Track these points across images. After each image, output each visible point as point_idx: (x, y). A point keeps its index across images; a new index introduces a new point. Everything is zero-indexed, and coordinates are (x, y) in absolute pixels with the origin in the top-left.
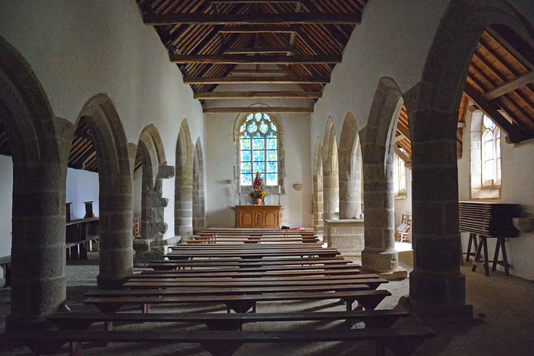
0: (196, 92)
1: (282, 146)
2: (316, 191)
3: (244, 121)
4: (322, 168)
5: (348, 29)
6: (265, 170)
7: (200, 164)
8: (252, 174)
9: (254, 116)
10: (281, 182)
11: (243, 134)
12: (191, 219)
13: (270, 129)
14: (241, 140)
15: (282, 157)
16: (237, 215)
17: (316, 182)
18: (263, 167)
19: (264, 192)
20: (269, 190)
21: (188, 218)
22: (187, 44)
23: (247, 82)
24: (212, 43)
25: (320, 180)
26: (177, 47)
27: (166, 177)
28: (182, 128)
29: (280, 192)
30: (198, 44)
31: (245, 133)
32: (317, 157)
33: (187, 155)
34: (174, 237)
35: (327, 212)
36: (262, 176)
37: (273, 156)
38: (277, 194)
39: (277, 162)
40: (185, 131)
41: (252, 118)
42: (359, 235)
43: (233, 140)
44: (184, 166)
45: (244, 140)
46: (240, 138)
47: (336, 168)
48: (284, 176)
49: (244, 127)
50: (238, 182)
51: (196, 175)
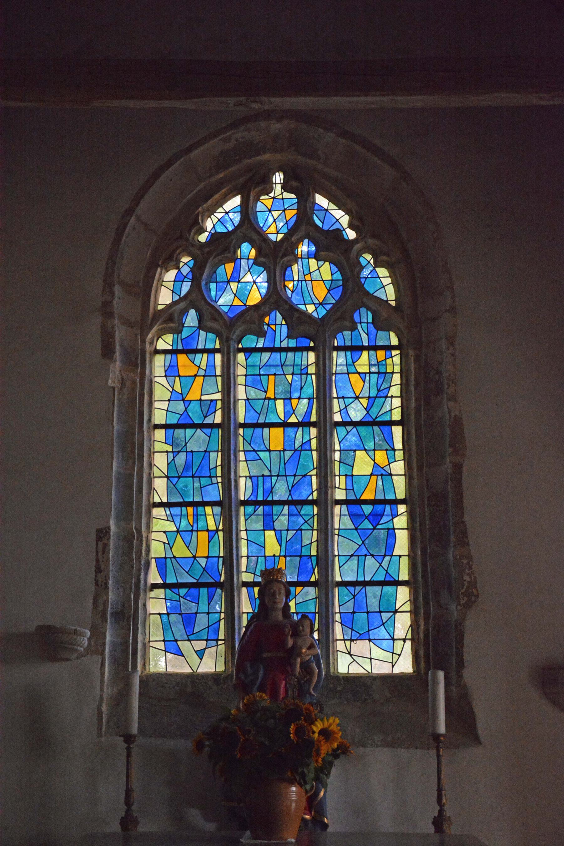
1: (439, 391)
3: (181, 237)
5: (104, 729)
11: (170, 319)
15: (447, 466)
19: (333, 723)
29: (442, 729)
31: (185, 312)
41: (236, 218)
43: (98, 351)
46: (148, 348)
48: (468, 606)
49: (179, 279)
50: (125, 643)
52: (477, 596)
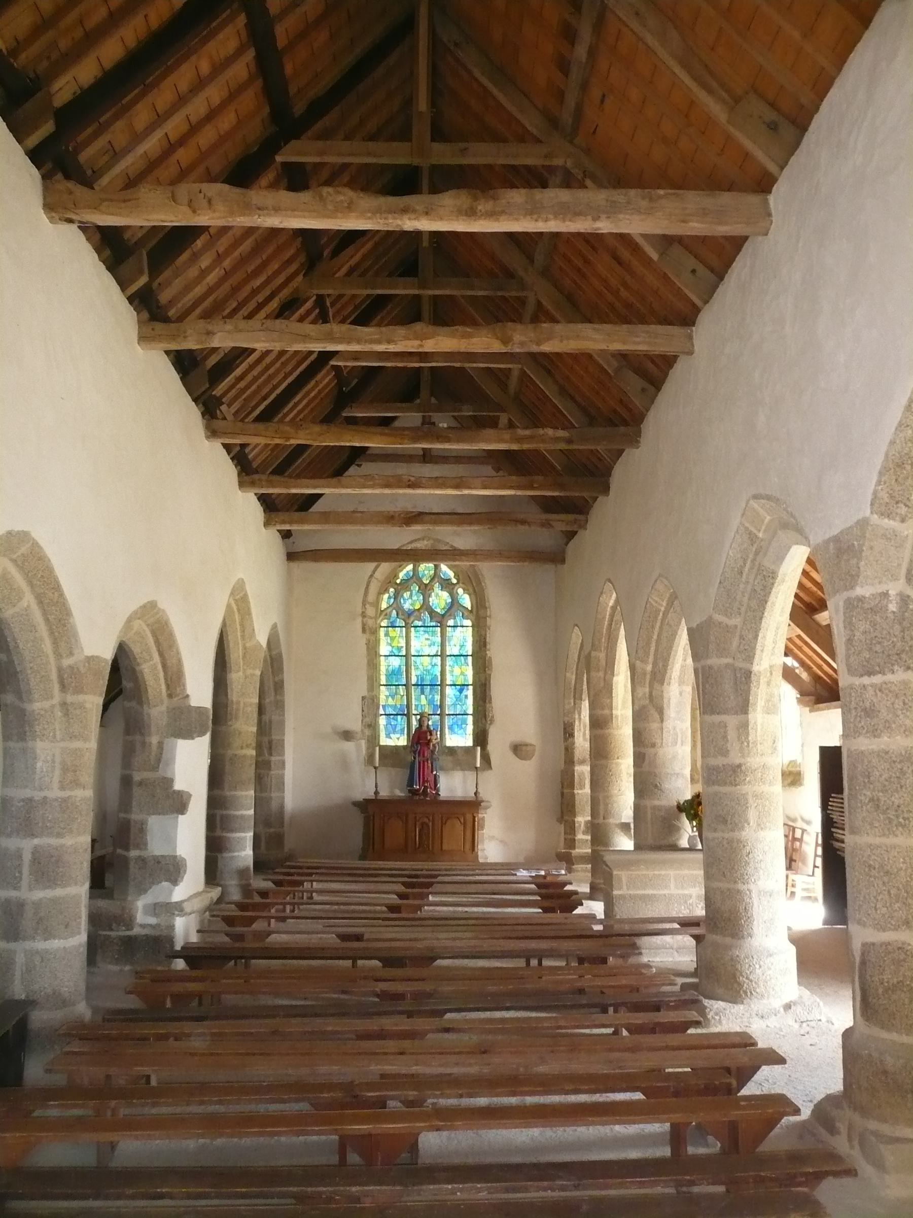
0: (269, 504)
2: (570, 761)
4: (585, 705)
6: (442, 706)
7: (276, 690)
8: (408, 716)
9: (415, 570)
10: (481, 738)
12: (250, 835)
13: (454, 604)
14: (382, 629)
16: (368, 823)
17: (570, 740)
18: (437, 697)
20: (450, 758)
21: (243, 835)
22: (248, 392)
23: (401, 491)
24: (313, 389)
25: (581, 734)
26: (224, 400)
27: (188, 734)
28: (233, 602)
29: (478, 765)
30: (278, 391)
32: (574, 677)
33: (244, 670)
34: (203, 891)
35: (601, 821)
36: (432, 722)
37: (464, 672)
38: (470, 769)
39: (471, 688)
40: (239, 610)
42: (686, 892)
44: (234, 700)
45: (390, 629)
47: (624, 707)
49: (389, 598)
51: (265, 718)
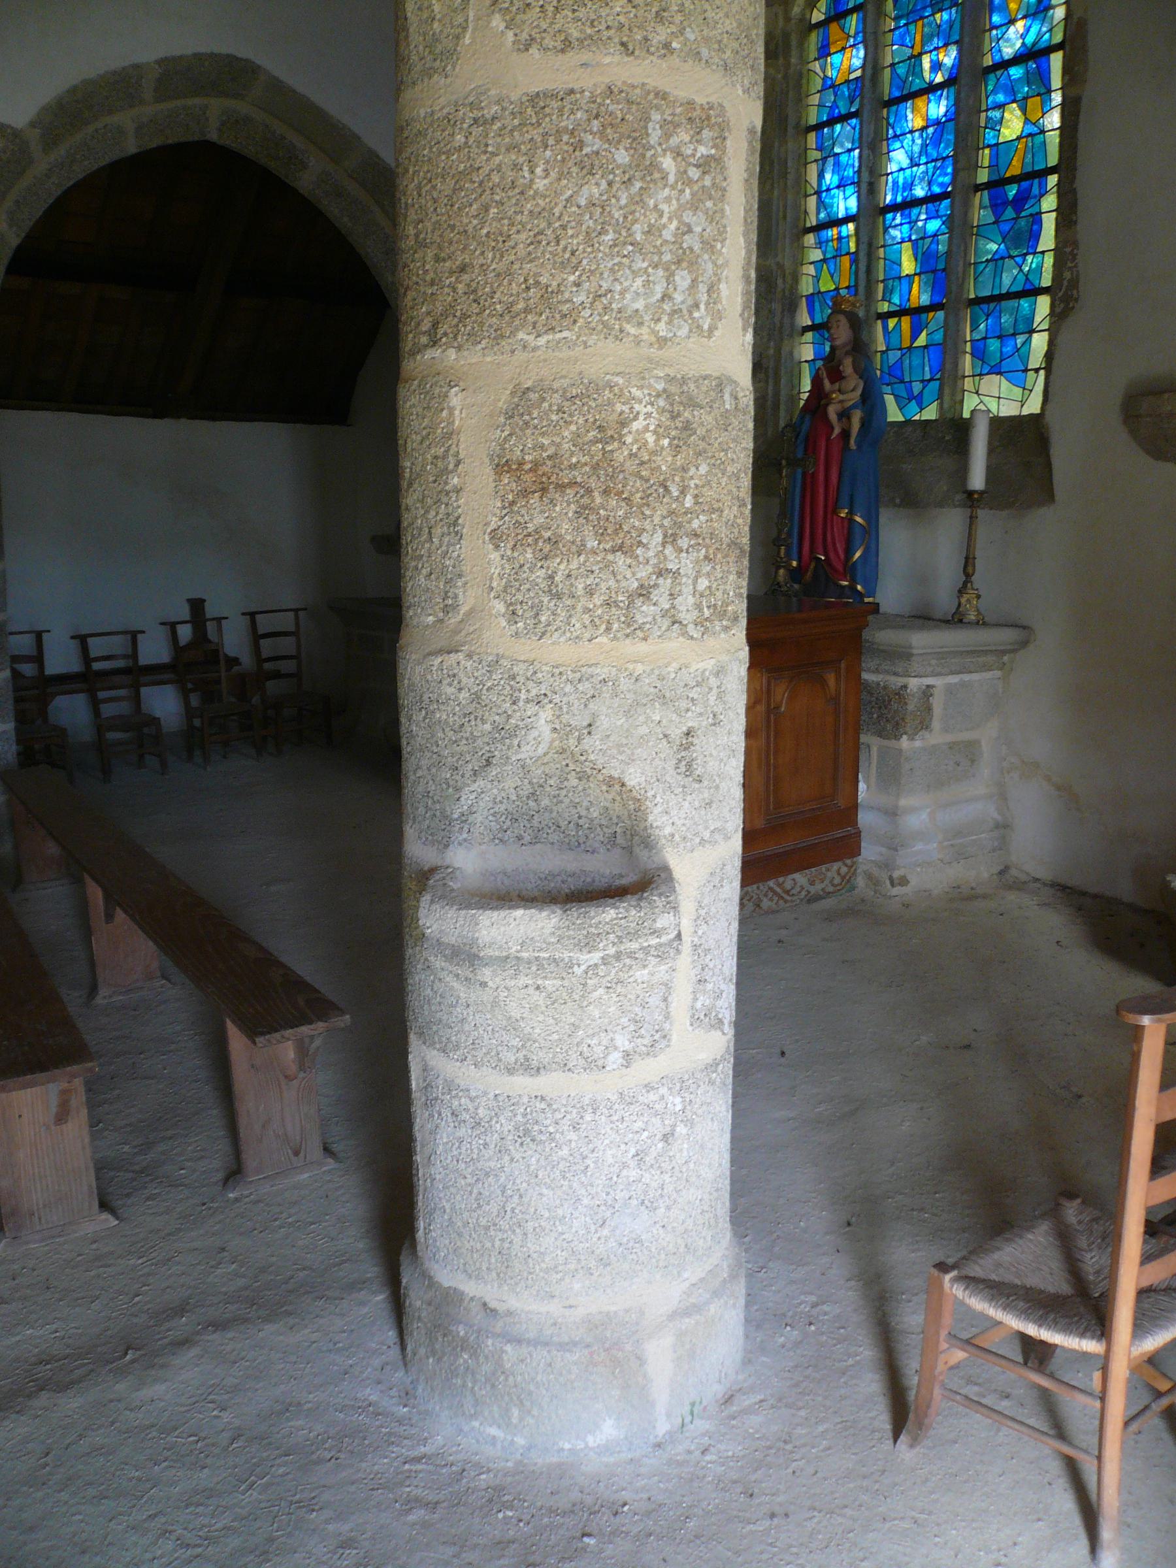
52: (1077, 300)
